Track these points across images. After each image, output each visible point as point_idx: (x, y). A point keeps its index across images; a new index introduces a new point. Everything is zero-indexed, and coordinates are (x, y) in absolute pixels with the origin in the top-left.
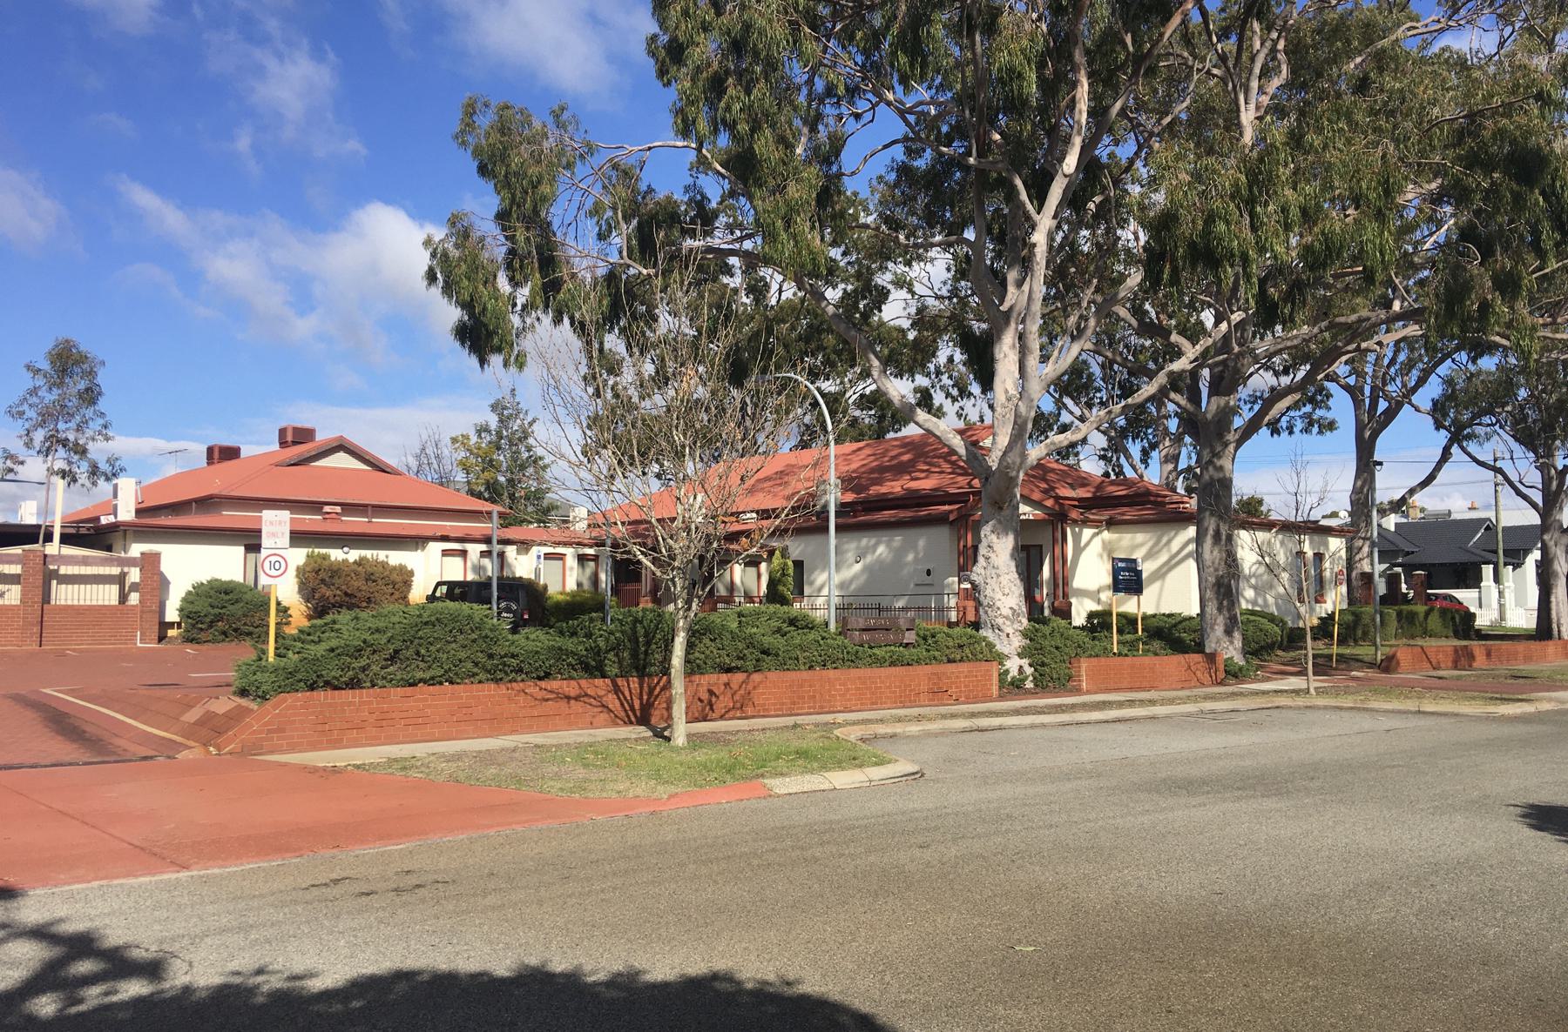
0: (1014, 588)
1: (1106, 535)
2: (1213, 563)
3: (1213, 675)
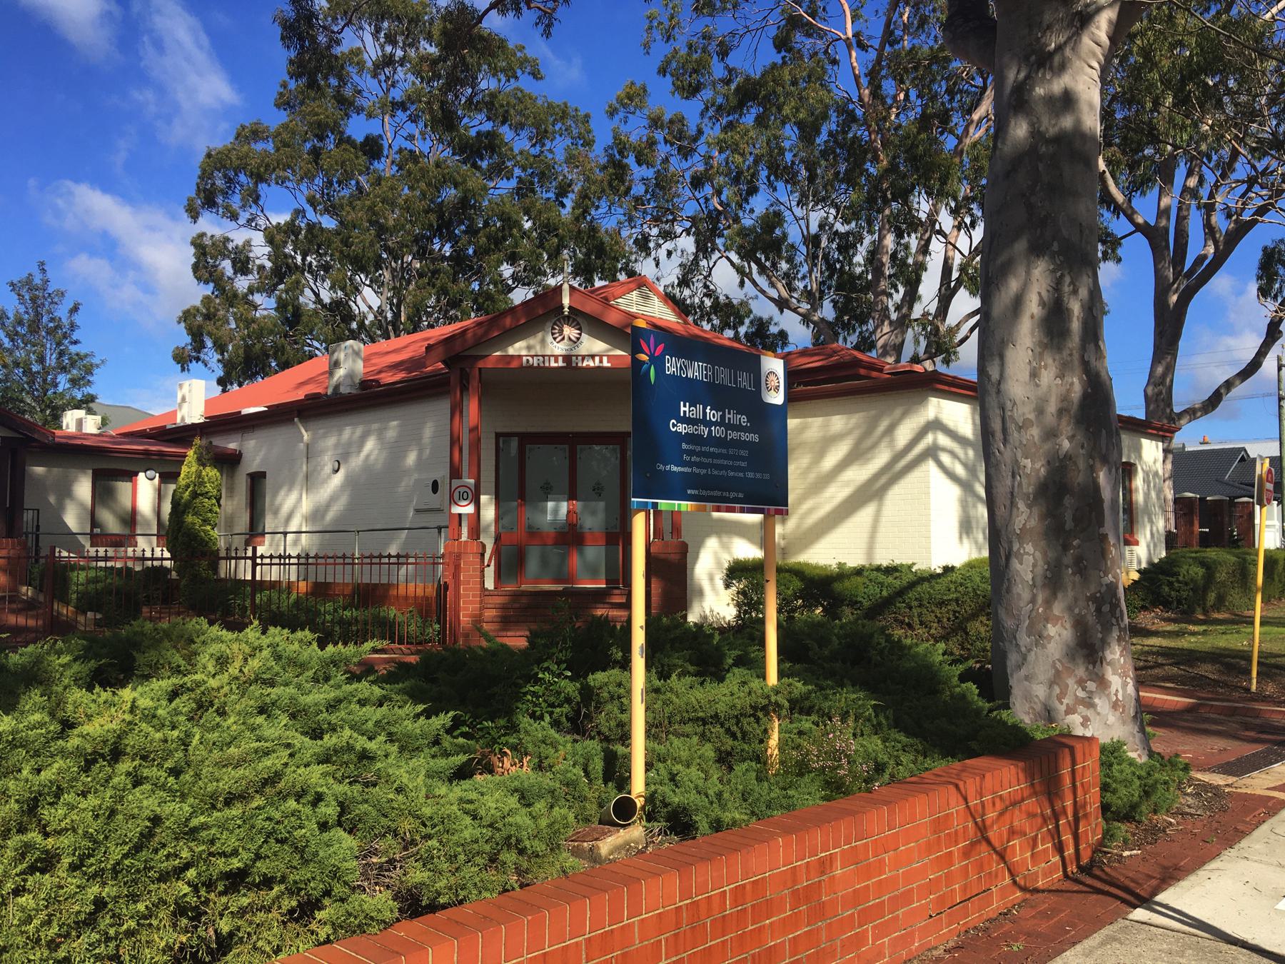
2: (1040, 411)
3: (1067, 837)
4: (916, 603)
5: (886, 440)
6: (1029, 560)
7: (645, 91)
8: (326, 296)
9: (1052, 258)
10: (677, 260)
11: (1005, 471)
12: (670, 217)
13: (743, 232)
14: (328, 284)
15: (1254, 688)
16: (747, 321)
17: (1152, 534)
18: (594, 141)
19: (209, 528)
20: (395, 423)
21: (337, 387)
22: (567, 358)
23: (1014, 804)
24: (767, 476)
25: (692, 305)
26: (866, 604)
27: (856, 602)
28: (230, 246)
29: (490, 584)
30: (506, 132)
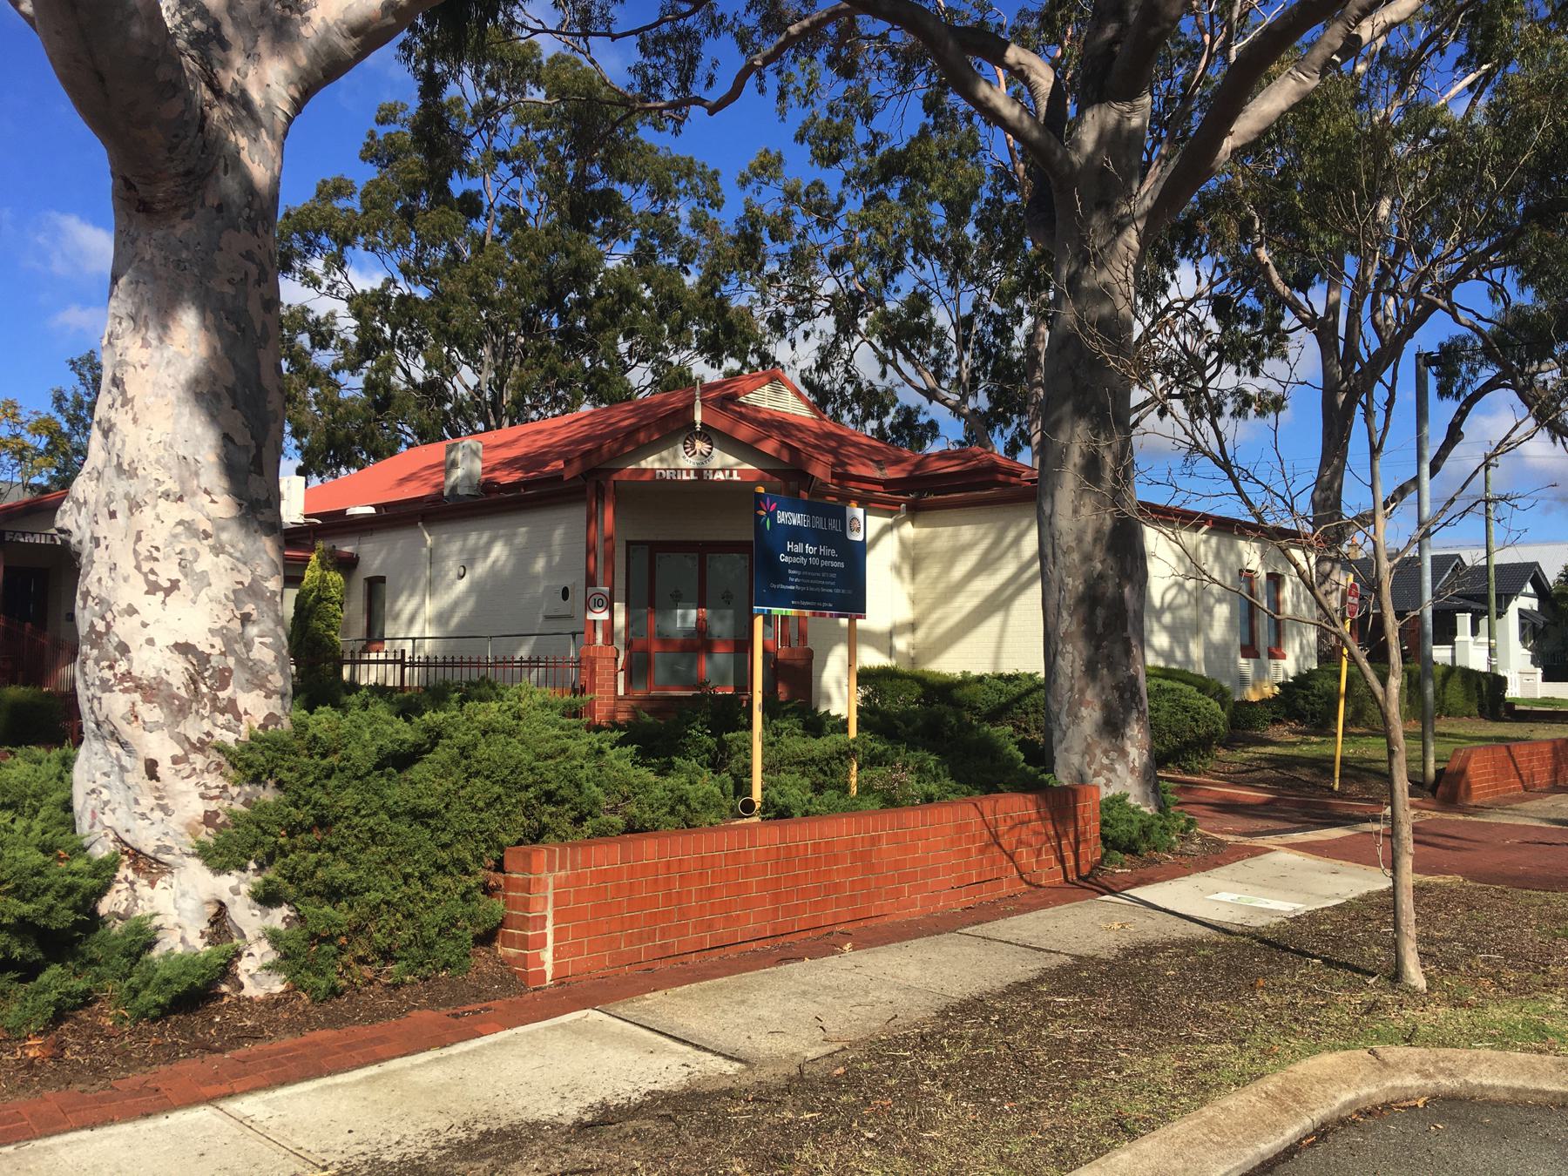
0: (206, 561)
1: (909, 530)
2: (1080, 540)
3: (1068, 854)
4: (1032, 709)
5: (1014, 550)
6: (1069, 657)
7: (780, 160)
8: (418, 375)
9: (1091, 420)
10: (814, 341)
11: (1054, 586)
12: (807, 295)
13: (886, 317)
14: (422, 362)
15: (1336, 787)
16: (892, 411)
17: (1302, 648)
18: (723, 201)
19: (333, 633)
20: (523, 530)
21: (454, 488)
22: (699, 472)
23: (1022, 823)
24: (850, 592)
25: (832, 392)
26: (985, 709)
27: (976, 708)
28: (311, 317)
29: (621, 692)
30: (625, 190)
